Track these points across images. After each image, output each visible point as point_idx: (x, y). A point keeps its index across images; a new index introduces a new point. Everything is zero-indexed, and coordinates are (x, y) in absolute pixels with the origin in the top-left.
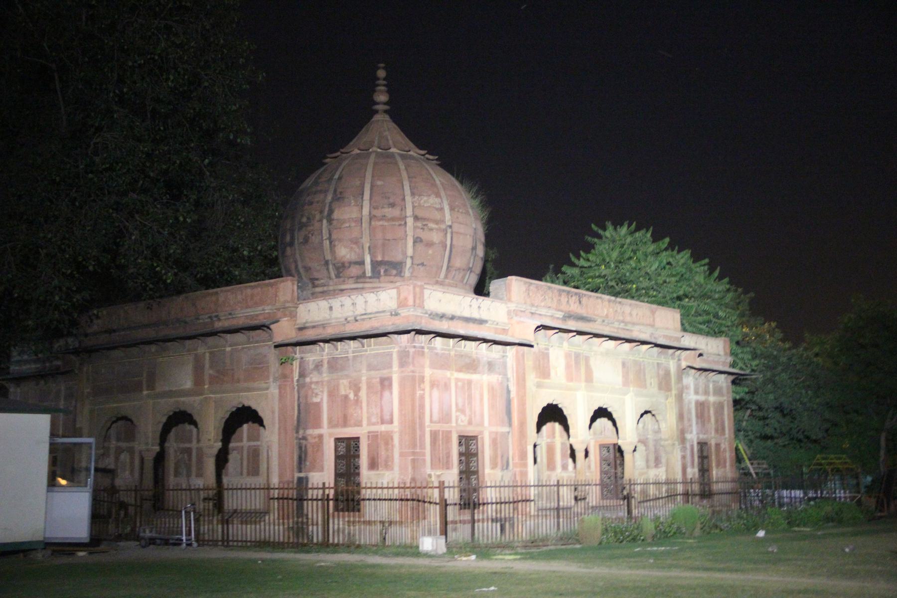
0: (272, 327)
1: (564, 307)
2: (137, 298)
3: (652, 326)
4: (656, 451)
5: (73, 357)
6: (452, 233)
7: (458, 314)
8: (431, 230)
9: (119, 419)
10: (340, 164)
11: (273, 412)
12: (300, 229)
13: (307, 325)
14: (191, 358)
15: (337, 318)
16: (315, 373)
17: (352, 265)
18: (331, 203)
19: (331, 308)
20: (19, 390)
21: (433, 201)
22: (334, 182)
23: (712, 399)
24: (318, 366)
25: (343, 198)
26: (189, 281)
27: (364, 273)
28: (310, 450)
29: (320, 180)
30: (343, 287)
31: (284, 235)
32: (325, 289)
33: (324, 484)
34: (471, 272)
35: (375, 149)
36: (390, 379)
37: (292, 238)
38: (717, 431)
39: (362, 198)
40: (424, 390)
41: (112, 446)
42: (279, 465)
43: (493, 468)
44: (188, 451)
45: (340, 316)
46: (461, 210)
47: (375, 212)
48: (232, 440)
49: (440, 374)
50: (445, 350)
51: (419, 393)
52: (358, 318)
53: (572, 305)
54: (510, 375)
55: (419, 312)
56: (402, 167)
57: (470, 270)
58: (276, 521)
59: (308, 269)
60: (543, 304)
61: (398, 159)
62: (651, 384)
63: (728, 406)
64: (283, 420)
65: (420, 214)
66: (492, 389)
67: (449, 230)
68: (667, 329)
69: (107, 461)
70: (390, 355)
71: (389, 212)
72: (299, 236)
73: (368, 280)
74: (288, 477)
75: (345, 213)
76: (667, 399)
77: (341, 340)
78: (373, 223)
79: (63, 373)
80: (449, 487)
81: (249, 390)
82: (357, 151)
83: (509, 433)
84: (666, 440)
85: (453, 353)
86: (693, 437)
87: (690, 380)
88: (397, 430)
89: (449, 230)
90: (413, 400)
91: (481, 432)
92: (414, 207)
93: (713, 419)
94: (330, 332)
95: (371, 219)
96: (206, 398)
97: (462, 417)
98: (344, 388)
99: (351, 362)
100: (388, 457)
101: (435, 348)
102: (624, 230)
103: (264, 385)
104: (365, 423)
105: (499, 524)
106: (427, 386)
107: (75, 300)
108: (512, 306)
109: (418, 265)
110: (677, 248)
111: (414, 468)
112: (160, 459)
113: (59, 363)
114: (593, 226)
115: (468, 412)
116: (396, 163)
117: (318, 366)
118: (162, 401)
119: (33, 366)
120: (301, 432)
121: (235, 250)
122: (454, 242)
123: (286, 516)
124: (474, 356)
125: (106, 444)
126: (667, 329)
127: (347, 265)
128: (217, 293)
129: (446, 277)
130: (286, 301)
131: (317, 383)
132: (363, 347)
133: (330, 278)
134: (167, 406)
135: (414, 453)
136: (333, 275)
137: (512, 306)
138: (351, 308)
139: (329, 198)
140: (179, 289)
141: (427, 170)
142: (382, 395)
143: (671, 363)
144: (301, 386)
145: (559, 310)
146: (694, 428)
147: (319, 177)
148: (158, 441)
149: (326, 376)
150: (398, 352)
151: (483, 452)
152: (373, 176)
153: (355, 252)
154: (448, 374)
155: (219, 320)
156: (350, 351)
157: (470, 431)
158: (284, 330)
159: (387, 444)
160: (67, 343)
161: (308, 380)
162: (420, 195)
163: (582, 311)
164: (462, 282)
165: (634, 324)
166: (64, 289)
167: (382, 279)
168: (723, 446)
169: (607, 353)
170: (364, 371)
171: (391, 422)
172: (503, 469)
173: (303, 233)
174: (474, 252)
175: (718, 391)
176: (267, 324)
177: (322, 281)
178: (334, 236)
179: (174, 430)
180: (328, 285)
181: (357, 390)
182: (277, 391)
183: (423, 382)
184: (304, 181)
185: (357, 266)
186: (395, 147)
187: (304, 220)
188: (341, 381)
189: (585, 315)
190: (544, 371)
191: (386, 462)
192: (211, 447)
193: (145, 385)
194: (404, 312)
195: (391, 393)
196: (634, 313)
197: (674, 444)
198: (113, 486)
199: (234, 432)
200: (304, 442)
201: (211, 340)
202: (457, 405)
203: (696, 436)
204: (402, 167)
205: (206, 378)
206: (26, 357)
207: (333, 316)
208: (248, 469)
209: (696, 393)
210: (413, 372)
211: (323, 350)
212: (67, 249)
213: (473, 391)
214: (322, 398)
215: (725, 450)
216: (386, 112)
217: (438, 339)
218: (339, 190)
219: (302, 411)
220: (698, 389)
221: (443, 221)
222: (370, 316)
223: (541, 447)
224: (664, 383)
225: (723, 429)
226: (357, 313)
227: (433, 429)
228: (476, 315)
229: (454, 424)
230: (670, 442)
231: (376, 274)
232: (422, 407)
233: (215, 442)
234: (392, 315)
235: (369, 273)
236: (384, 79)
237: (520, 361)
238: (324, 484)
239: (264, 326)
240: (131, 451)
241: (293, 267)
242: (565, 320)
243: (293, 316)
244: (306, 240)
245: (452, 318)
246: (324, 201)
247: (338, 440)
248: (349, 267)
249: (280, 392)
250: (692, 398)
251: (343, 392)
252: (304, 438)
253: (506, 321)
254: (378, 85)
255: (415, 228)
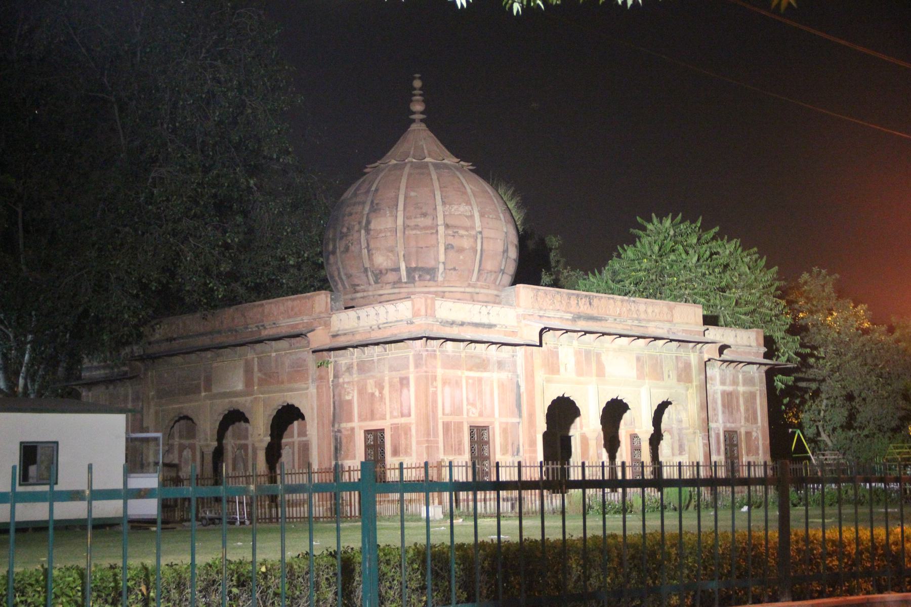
0: (308, 335)
1: (574, 309)
2: (192, 309)
3: (671, 321)
4: (680, 440)
5: (138, 363)
6: (482, 238)
7: (468, 320)
8: (462, 236)
9: (181, 418)
10: (377, 175)
11: (312, 409)
12: (341, 238)
13: (339, 333)
14: (242, 362)
15: (364, 327)
16: (347, 374)
17: (389, 272)
18: (368, 214)
19: (359, 318)
20: (90, 394)
21: (463, 209)
22: (371, 194)
23: (741, 389)
24: (349, 368)
25: (380, 209)
26: (241, 291)
27: (400, 279)
28: (344, 441)
29: (358, 192)
30: (381, 292)
31: (327, 244)
32: (365, 294)
33: (350, 467)
34: (503, 274)
35: (410, 159)
36: (407, 379)
37: (335, 247)
38: (747, 420)
39: (397, 209)
40: (436, 387)
41: (176, 443)
42: (319, 453)
43: (503, 454)
44: (245, 447)
45: (366, 324)
46: (491, 216)
47: (408, 222)
48: (284, 436)
49: (451, 373)
50: (457, 352)
51: (431, 389)
52: (381, 326)
53: (582, 307)
54: (519, 372)
55: (430, 321)
56: (434, 177)
57: (503, 272)
58: (317, 503)
59: (349, 276)
60: (551, 307)
61: (432, 168)
62: (669, 376)
63: (760, 396)
64: (320, 416)
65: (450, 222)
66: (502, 385)
67: (479, 236)
68: (687, 323)
69: (171, 456)
70: (407, 358)
71: (422, 221)
72: (340, 246)
73: (404, 285)
74: (326, 465)
75: (381, 223)
76: (687, 390)
77: (366, 345)
78: (406, 232)
79: (130, 378)
80: (458, 466)
81: (292, 390)
82: (394, 162)
83: (519, 423)
84: (687, 429)
85: (463, 355)
86: (719, 425)
87: (715, 371)
88: (414, 421)
89: (479, 236)
90: (427, 396)
91: (492, 423)
92: (445, 216)
93: (742, 408)
94: (358, 339)
95: (404, 229)
96: (256, 398)
97: (474, 410)
98: (371, 388)
99: (376, 364)
100: (407, 445)
101: (447, 351)
102: (667, 222)
103: (305, 386)
104: (388, 416)
105: (509, 503)
106: (439, 384)
107: (141, 316)
108: (520, 311)
109: (450, 270)
110: (726, 237)
111: (428, 454)
112: (219, 454)
113: (126, 369)
114: (638, 219)
115: (478, 404)
116: (429, 174)
117: (349, 368)
118: (218, 401)
119: (102, 372)
120: (336, 426)
121: (283, 259)
122: (485, 247)
123: (325, 499)
124: (484, 356)
125: (170, 442)
126: (687, 323)
127: (384, 272)
128: (262, 305)
129: (478, 279)
130: (321, 312)
131: (348, 383)
132: (386, 351)
133: (370, 284)
134: (222, 406)
135: (428, 441)
136: (372, 282)
137: (520, 311)
138: (375, 318)
139: (367, 209)
140: (232, 300)
141: (459, 178)
142: (401, 392)
143: (693, 357)
144: (336, 386)
145: (568, 312)
146: (720, 418)
147: (358, 189)
148: (216, 437)
149: (355, 377)
150: (414, 355)
151: (494, 441)
152: (407, 188)
153: (391, 259)
154: (459, 373)
155: (265, 328)
156: (375, 355)
157: (481, 422)
158: (319, 338)
159: (406, 434)
160: (132, 352)
161: (341, 380)
162: (450, 204)
163: (593, 312)
164: (495, 283)
165: (649, 321)
166: (132, 308)
167: (417, 284)
168: (754, 434)
169: (621, 349)
170: (387, 372)
171: (409, 415)
172: (513, 455)
173: (343, 243)
174: (505, 255)
175: (749, 381)
176: (304, 333)
177: (362, 287)
178: (372, 245)
179: (230, 428)
180: (368, 291)
181: (381, 389)
182: (315, 391)
183: (436, 380)
184: (342, 195)
185: (394, 273)
186: (430, 156)
187: (345, 230)
188: (368, 381)
189: (596, 315)
190: (553, 367)
191: (406, 449)
192: (261, 441)
193: (202, 389)
194: (417, 321)
195: (409, 390)
196: (650, 310)
197: (695, 433)
198: (178, 477)
199: (285, 429)
200: (339, 434)
201: (258, 347)
202: (467, 399)
203: (723, 425)
204: (434, 176)
205: (256, 380)
206: (95, 364)
207: (361, 324)
208: (299, 462)
209: (723, 383)
210: (426, 372)
211: (353, 354)
212: (133, 272)
213: (483, 387)
214: (352, 396)
215: (757, 438)
216: (422, 120)
217: (448, 342)
218: (375, 202)
219: (336, 407)
220: (725, 379)
221: (473, 228)
222: (390, 325)
223: (575, 438)
224: (684, 375)
225: (755, 419)
226: (380, 322)
227: (446, 420)
228: (485, 321)
229: (465, 416)
230: (691, 430)
231: (411, 279)
232: (435, 402)
233: (264, 436)
234: (408, 323)
235: (404, 279)
236: (420, 89)
237: (529, 360)
238: (350, 467)
239: (302, 334)
240: (192, 448)
241: (336, 273)
242: (575, 321)
243: (327, 325)
244: (347, 249)
245: (462, 324)
246: (362, 212)
247: (367, 432)
248: (387, 273)
249: (318, 392)
250: (717, 388)
251: (370, 391)
252: (339, 431)
253: (515, 324)
254: (415, 95)
255: (446, 236)
